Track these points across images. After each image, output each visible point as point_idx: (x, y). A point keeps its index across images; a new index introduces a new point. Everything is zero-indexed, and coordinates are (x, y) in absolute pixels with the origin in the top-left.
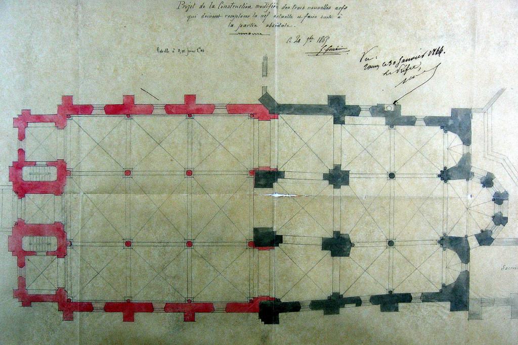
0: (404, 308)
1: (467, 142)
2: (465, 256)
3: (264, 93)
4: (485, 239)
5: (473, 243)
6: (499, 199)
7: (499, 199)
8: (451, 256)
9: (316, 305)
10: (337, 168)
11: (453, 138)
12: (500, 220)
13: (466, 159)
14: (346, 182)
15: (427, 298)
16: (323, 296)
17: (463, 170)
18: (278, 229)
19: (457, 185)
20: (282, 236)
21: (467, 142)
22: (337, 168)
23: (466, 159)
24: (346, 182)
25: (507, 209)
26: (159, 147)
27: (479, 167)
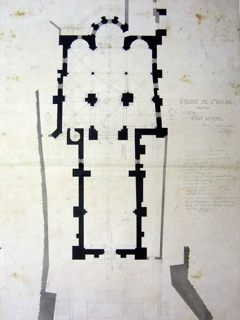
0: (124, 149)
1: (75, 38)
2: (133, 38)
3: (51, 136)
4: (125, 28)
5: (128, 34)
6: (104, 21)
7: (104, 21)
8: (134, 44)
9: (158, 110)
10: (86, 100)
11: (74, 44)
12: (115, 21)
13: (84, 38)
14: (94, 95)
15: (155, 56)
16: (153, 105)
17: (91, 40)
18: (120, 128)
19: (97, 41)
20: (123, 126)
21: (75, 38)
22: (86, 100)
23: (84, 38)
24: (94, 95)
25: (110, 17)
26: (207, 53)
27: (89, 31)
